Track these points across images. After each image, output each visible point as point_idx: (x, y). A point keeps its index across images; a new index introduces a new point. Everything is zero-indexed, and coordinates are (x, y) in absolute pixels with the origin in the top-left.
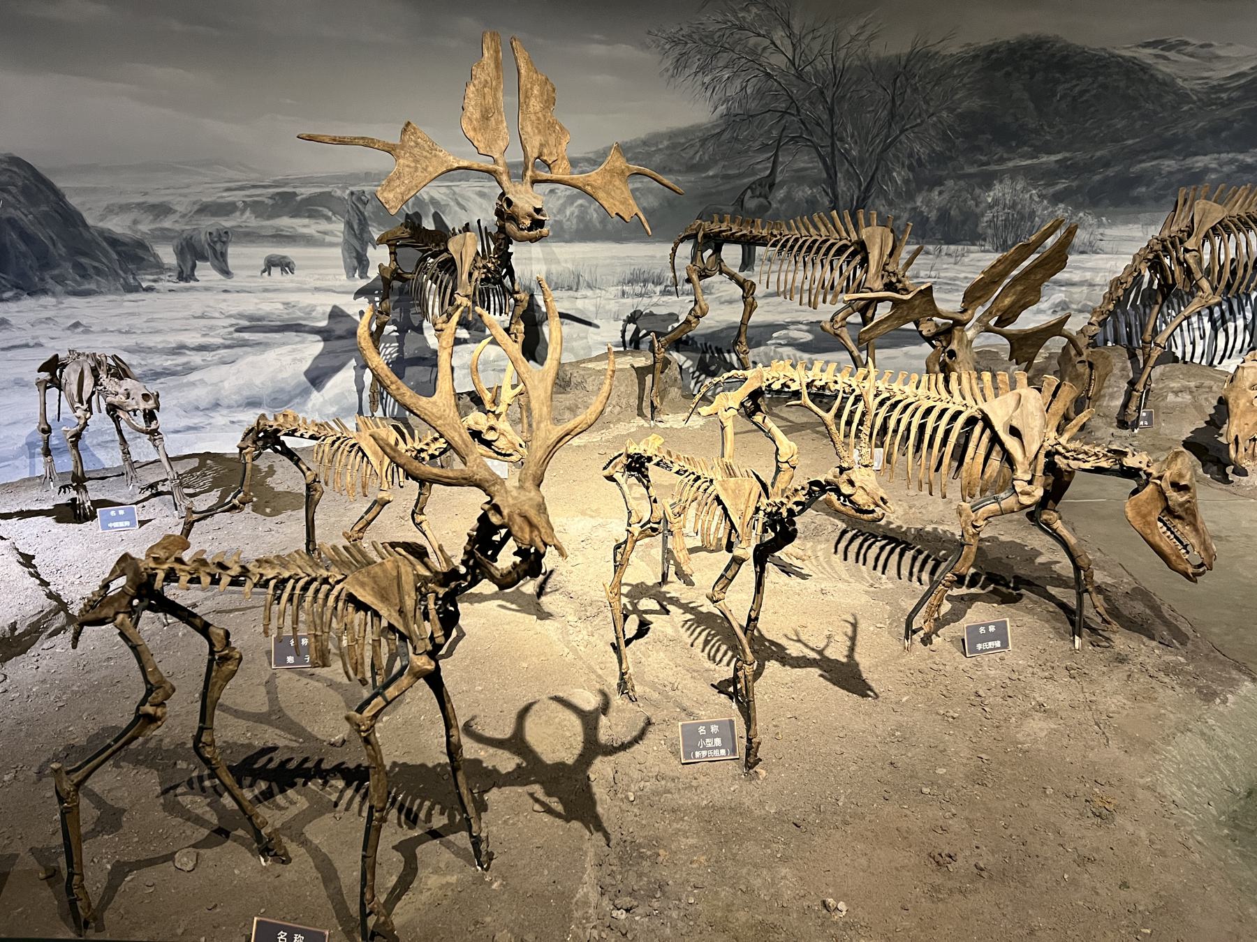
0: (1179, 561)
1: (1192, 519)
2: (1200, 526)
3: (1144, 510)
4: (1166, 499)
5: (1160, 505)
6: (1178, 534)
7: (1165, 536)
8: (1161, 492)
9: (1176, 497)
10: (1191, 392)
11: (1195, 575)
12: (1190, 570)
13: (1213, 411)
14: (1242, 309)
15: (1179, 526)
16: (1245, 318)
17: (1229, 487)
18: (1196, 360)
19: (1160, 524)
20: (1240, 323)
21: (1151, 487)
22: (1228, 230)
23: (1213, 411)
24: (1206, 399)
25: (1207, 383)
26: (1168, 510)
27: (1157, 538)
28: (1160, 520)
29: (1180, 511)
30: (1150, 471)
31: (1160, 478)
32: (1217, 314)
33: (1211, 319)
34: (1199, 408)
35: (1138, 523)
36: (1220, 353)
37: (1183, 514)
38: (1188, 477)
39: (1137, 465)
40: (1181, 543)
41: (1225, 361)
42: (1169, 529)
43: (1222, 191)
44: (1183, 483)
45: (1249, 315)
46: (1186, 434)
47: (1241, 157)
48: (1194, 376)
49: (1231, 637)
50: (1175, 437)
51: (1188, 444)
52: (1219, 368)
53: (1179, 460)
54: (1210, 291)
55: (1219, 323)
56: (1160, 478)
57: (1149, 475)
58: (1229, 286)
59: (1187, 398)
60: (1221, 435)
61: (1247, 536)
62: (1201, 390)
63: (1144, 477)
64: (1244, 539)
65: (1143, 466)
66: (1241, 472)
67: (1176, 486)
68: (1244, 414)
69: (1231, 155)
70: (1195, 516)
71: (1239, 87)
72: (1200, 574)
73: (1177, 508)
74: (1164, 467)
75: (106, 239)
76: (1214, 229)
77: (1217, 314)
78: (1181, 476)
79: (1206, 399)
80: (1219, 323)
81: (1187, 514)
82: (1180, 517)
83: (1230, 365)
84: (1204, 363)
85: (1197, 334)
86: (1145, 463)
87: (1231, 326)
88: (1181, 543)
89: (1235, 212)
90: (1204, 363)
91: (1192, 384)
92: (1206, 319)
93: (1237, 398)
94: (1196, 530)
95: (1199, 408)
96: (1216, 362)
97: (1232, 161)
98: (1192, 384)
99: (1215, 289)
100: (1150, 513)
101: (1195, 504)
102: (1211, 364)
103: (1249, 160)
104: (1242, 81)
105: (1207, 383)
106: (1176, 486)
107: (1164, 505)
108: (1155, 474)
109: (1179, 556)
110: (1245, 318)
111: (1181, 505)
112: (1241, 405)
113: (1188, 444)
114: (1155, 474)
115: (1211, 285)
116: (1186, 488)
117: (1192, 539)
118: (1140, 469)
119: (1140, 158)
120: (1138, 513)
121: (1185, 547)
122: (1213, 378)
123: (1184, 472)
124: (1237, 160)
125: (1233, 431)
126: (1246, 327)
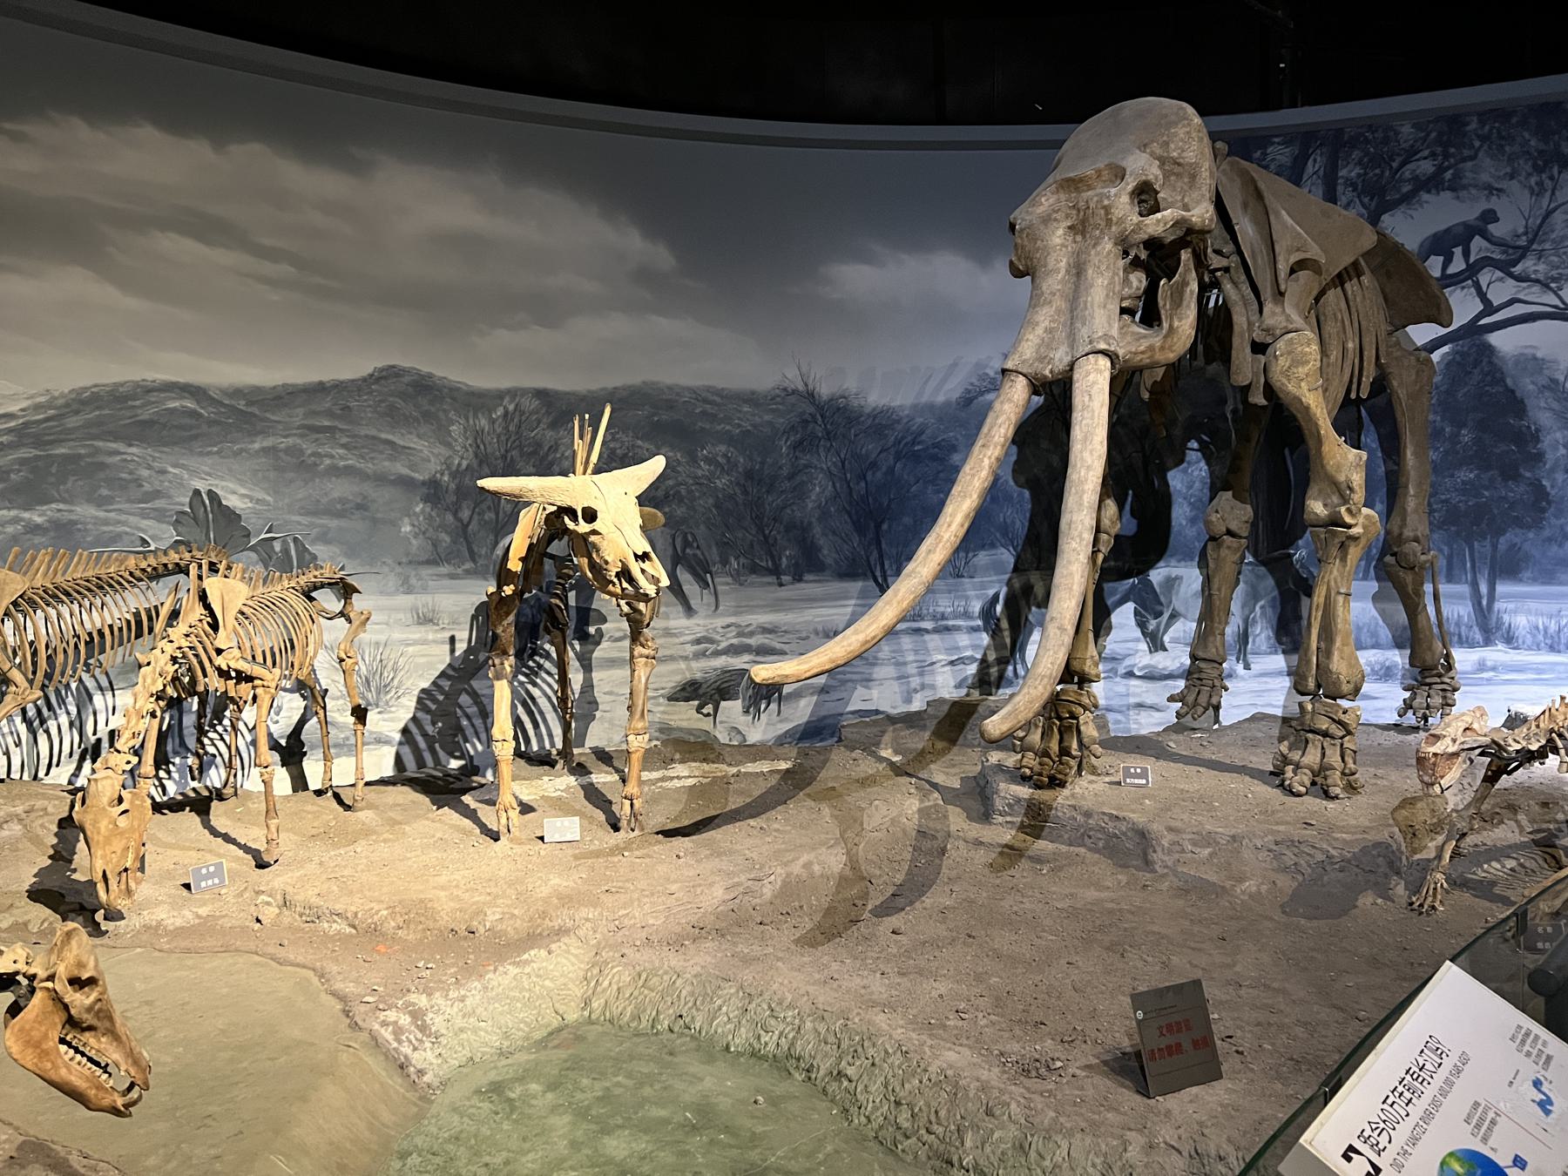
0: (101, 1094)
1: (108, 1024)
2: (120, 1029)
3: (36, 1034)
4: (66, 1007)
5: (59, 1019)
6: (92, 1054)
7: (73, 1064)
8: (57, 999)
9: (79, 1001)
10: (20, 820)
11: (127, 1106)
12: (120, 1102)
13: (55, 841)
14: (62, 702)
15: (92, 1041)
16: (68, 713)
17: (105, 940)
18: (15, 775)
19: (63, 1048)
20: (64, 720)
21: (39, 995)
22: (33, 605)
23: (55, 841)
24: (42, 826)
25: (39, 804)
26: (72, 1022)
27: (63, 1072)
28: (62, 1041)
29: (89, 1019)
30: (32, 971)
31: (51, 978)
32: (31, 712)
33: (25, 719)
34: (36, 841)
35: (29, 1059)
36: (44, 762)
37: (95, 1022)
38: (92, 964)
39: (11, 968)
40: (97, 1064)
41: (53, 770)
42: (77, 1051)
43: (16, 557)
44: (85, 976)
45: (73, 710)
46: (28, 880)
47: (26, 515)
48: (19, 796)
49: (174, 1164)
50: (14, 888)
51: (35, 895)
52: (47, 780)
53: (74, 943)
54: (26, 684)
55: (36, 723)
56: (51, 978)
57: (32, 978)
58: (49, 676)
59: (16, 828)
60: (75, 871)
61: (147, 1003)
62: (33, 815)
63: (25, 982)
64: (146, 1009)
65: (21, 967)
66: (114, 915)
67: (77, 983)
68: (108, 841)
69: (13, 513)
70: (111, 1019)
71: (10, 431)
72: (134, 1103)
73: (85, 1016)
74: (54, 958)
75: (713, 394)
76: (15, 603)
77: (31, 712)
78: (81, 965)
79: (42, 826)
80: (36, 723)
81: (102, 1021)
82: (91, 1028)
83: (61, 775)
84: (26, 777)
85: (10, 740)
86: (22, 960)
87: (52, 725)
88: (97, 1064)
89: (38, 582)
90: (26, 777)
91: (20, 809)
92: (18, 720)
93: (96, 821)
94: (115, 1037)
95: (36, 841)
96: (41, 774)
97: (16, 520)
98: (20, 809)
99: (31, 682)
100: (46, 1036)
101: (108, 1001)
102: (35, 777)
103: (39, 520)
104: (13, 424)
105: (39, 804)
106: (77, 983)
107: (64, 1016)
108: (42, 974)
109: (100, 1087)
110: (68, 713)
111: (89, 1009)
112: (103, 830)
113: (35, 895)
114: (42, 974)
115: (25, 675)
116: (92, 981)
117: (113, 1054)
118: (17, 973)
119: (1305, 614)
120: (28, 1044)
121: (105, 1069)
122: (45, 797)
123: (84, 959)
124: (22, 519)
125: (99, 866)
126: (71, 724)
